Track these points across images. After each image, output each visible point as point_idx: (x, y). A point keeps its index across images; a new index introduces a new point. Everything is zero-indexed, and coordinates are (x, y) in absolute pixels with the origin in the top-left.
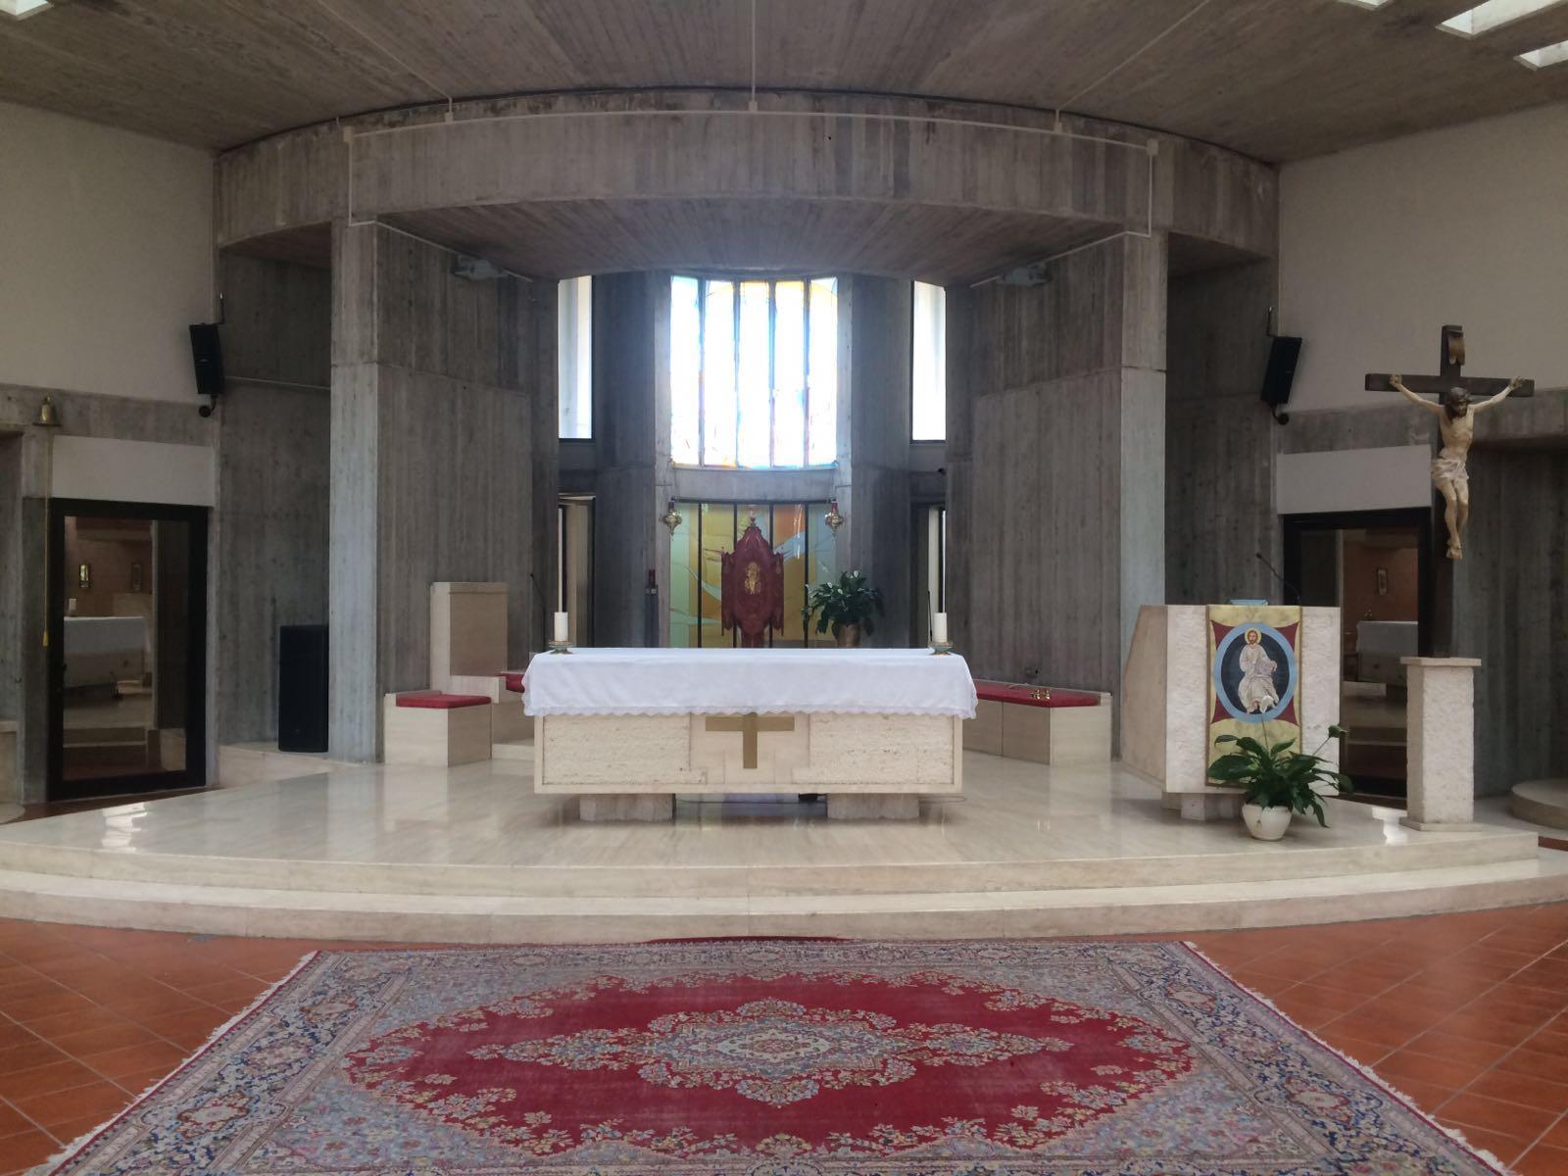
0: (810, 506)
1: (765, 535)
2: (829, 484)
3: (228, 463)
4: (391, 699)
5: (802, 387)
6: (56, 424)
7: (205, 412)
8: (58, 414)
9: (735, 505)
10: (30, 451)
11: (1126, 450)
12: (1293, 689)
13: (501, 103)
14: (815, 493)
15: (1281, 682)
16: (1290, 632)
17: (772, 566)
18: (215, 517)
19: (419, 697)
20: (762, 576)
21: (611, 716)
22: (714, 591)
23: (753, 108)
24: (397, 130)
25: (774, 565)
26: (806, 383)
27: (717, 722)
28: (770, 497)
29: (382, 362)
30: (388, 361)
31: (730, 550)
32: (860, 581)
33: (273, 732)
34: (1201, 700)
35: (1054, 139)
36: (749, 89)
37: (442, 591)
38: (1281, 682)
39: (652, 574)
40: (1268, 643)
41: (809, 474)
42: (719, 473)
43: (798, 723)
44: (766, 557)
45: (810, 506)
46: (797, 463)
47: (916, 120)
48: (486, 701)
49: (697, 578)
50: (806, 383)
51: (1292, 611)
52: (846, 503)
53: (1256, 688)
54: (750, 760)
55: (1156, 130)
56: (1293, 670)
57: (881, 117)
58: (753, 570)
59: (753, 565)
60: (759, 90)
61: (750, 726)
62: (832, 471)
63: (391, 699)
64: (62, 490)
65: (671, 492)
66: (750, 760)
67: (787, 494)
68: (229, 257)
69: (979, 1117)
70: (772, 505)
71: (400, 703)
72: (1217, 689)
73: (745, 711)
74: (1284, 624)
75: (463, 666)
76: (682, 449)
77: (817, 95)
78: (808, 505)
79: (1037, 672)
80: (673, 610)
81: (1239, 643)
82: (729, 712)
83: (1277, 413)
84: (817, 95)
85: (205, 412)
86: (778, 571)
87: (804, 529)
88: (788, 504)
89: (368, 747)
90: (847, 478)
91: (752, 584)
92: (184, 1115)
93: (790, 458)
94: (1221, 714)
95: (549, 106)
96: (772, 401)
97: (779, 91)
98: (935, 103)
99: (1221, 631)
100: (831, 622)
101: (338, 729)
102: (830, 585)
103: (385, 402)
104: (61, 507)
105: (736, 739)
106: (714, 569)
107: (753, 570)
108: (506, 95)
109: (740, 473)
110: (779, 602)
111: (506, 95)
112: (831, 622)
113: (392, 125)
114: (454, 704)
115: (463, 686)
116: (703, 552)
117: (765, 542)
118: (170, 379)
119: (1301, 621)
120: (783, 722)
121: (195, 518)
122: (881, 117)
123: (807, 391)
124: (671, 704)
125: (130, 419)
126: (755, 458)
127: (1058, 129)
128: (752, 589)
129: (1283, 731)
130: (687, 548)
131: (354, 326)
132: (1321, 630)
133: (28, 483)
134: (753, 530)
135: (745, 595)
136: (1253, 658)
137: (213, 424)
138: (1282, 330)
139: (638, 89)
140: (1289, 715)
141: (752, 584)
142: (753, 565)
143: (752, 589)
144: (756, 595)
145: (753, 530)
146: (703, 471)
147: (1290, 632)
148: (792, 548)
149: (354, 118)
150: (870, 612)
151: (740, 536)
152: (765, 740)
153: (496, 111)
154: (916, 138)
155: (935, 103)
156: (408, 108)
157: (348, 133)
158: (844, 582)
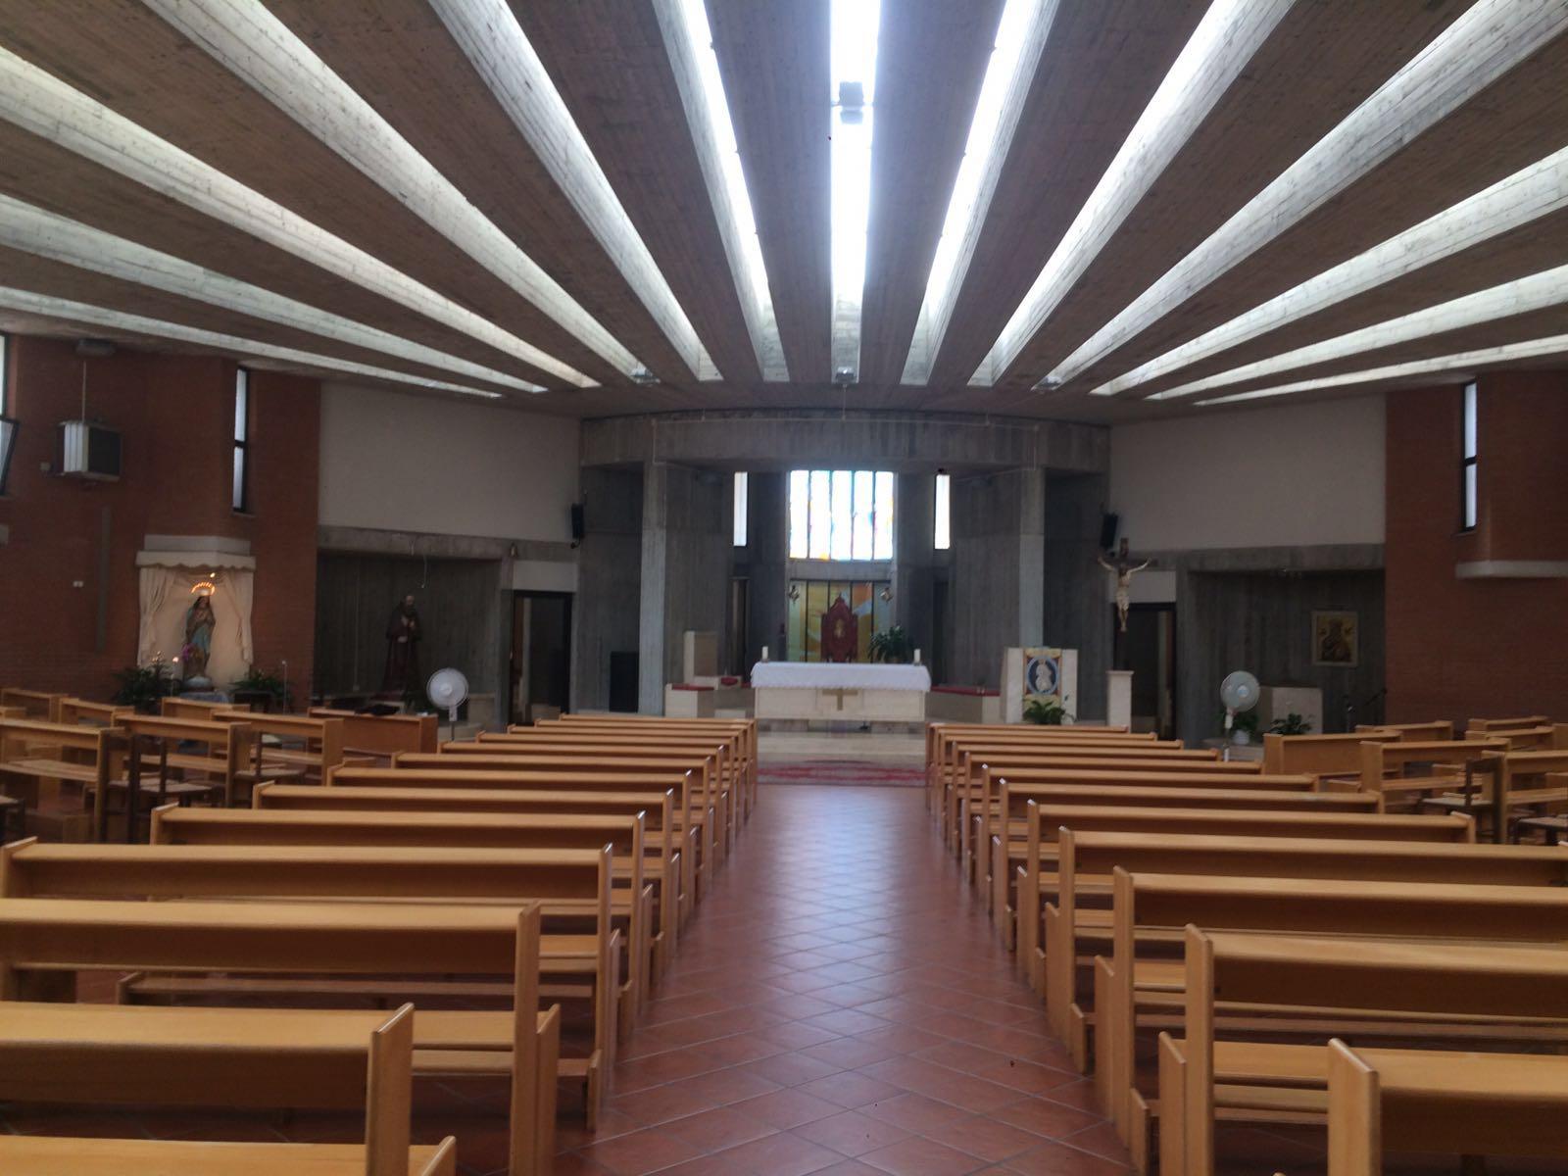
1: (847, 601)
2: (886, 571)
3: (583, 570)
4: (669, 686)
5: (871, 510)
6: (517, 556)
7: (573, 546)
8: (516, 550)
9: (830, 583)
10: (504, 567)
11: (1022, 573)
12: (1057, 682)
13: (728, 413)
14: (879, 576)
15: (1053, 679)
16: (1056, 660)
17: (851, 621)
18: (576, 598)
19: (680, 686)
20: (845, 628)
21: (784, 689)
22: (816, 635)
23: (844, 418)
24: (679, 422)
26: (873, 508)
27: (827, 692)
28: (851, 578)
29: (668, 528)
30: (671, 528)
31: (826, 611)
32: (901, 631)
33: (607, 703)
34: (1021, 686)
35: (986, 427)
36: (841, 409)
37: (690, 636)
38: (1053, 679)
39: (783, 626)
40: (1048, 664)
41: (874, 564)
42: (819, 563)
43: (859, 694)
46: (867, 557)
47: (919, 422)
48: (712, 689)
50: (873, 508)
51: (1057, 651)
52: (895, 584)
53: (1043, 682)
54: (840, 707)
55: (1039, 419)
56: (1057, 676)
57: (903, 421)
58: (839, 624)
60: (847, 410)
61: (840, 693)
62: (888, 563)
63: (669, 686)
64: (517, 585)
65: (793, 575)
66: (840, 707)
67: (861, 576)
68: (587, 472)
70: (852, 583)
71: (674, 688)
72: (1027, 682)
73: (838, 687)
74: (1054, 656)
75: (699, 672)
76: (797, 549)
77: (874, 412)
78: (875, 583)
81: (1036, 664)
82: (832, 688)
84: (874, 412)
85: (573, 546)
88: (862, 582)
89: (658, 709)
90: (894, 568)
91: (839, 632)
93: (863, 554)
94: (1029, 692)
95: (750, 416)
96: (853, 519)
97: (856, 410)
98: (928, 414)
99: (1029, 659)
100: (884, 654)
101: (644, 700)
102: (883, 634)
103: (668, 545)
104: (521, 594)
105: (834, 699)
106: (817, 622)
107: (839, 624)
108: (729, 410)
109: (831, 563)
110: (855, 642)
111: (729, 410)
112: (884, 654)
113: (675, 419)
114: (700, 689)
115: (701, 681)
116: (809, 613)
117: (847, 608)
118: (556, 529)
119: (1061, 656)
120: (854, 692)
121: (566, 598)
122: (903, 421)
123: (873, 514)
124: (809, 684)
125: (544, 551)
126: (841, 554)
127: (988, 423)
129: (1053, 698)
130: (801, 607)
131: (653, 512)
132: (1069, 659)
133: (503, 584)
134: (840, 600)
136: (1042, 670)
137: (577, 552)
138: (1111, 511)
139: (791, 409)
140: (1056, 692)
141: (839, 632)
145: (840, 600)
146: (808, 561)
147: (1056, 660)
148: (863, 609)
149: (655, 414)
150: (894, 651)
151: (832, 604)
152: (846, 699)
153: (725, 417)
155: (928, 414)
156: (685, 412)
157: (654, 422)
158: (892, 631)
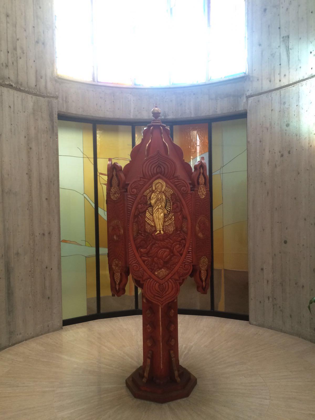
0: (214, 124)
20: (175, 204)
25: (194, 185)
44: (180, 173)
45: (214, 124)
49: (93, 205)
59: (160, 185)
69: (160, 109)
79: (22, 160)
80: (65, 241)
83: (111, 162)
86: (202, 192)
87: (207, 149)
91: (158, 218)
92: (136, 214)
128: (159, 225)
135: (147, 237)
142: (160, 185)
143: (159, 225)
144: (167, 236)
154: (132, 84)
